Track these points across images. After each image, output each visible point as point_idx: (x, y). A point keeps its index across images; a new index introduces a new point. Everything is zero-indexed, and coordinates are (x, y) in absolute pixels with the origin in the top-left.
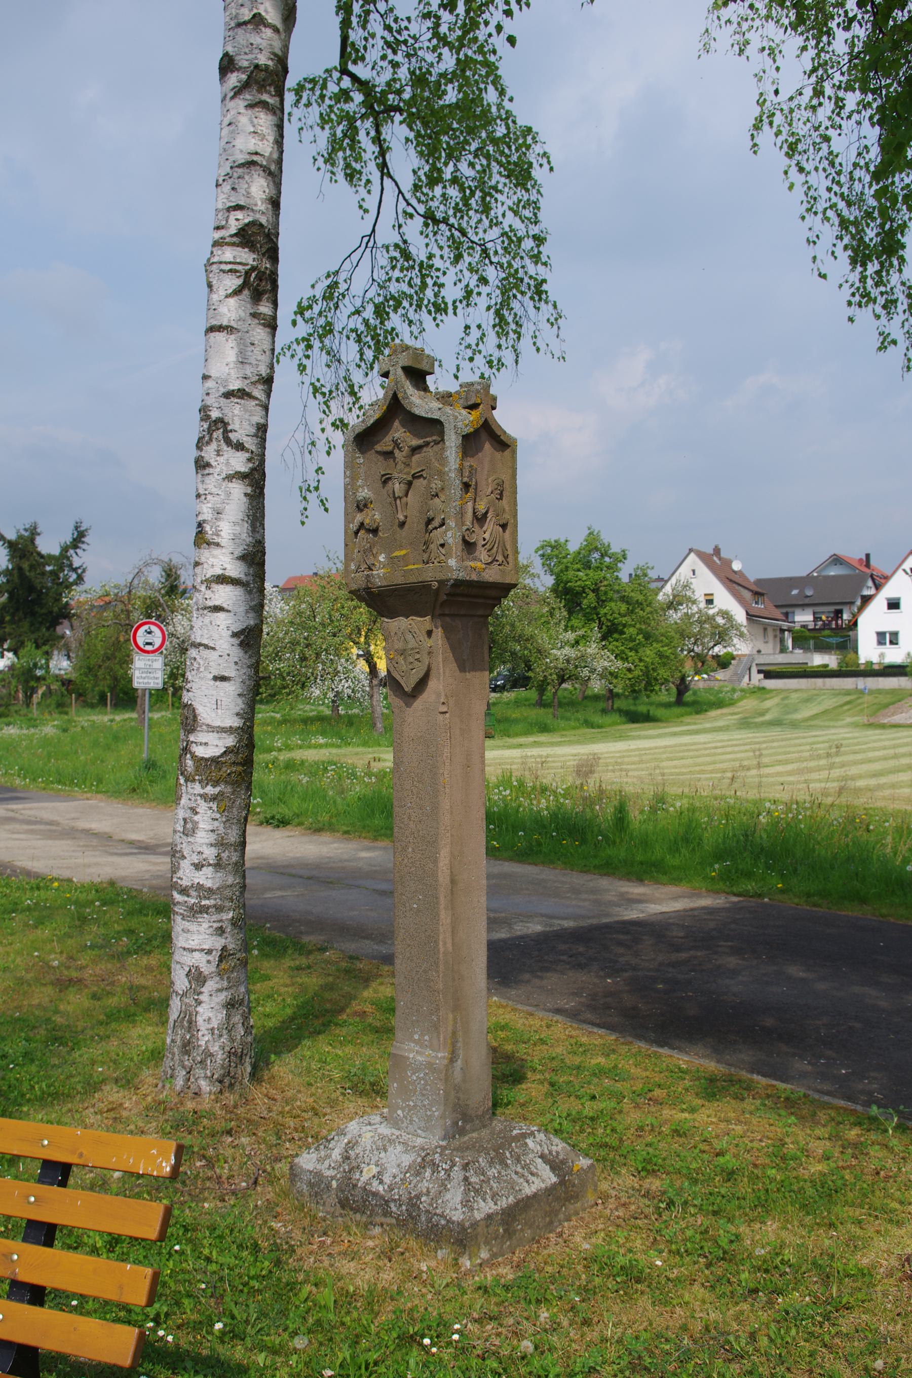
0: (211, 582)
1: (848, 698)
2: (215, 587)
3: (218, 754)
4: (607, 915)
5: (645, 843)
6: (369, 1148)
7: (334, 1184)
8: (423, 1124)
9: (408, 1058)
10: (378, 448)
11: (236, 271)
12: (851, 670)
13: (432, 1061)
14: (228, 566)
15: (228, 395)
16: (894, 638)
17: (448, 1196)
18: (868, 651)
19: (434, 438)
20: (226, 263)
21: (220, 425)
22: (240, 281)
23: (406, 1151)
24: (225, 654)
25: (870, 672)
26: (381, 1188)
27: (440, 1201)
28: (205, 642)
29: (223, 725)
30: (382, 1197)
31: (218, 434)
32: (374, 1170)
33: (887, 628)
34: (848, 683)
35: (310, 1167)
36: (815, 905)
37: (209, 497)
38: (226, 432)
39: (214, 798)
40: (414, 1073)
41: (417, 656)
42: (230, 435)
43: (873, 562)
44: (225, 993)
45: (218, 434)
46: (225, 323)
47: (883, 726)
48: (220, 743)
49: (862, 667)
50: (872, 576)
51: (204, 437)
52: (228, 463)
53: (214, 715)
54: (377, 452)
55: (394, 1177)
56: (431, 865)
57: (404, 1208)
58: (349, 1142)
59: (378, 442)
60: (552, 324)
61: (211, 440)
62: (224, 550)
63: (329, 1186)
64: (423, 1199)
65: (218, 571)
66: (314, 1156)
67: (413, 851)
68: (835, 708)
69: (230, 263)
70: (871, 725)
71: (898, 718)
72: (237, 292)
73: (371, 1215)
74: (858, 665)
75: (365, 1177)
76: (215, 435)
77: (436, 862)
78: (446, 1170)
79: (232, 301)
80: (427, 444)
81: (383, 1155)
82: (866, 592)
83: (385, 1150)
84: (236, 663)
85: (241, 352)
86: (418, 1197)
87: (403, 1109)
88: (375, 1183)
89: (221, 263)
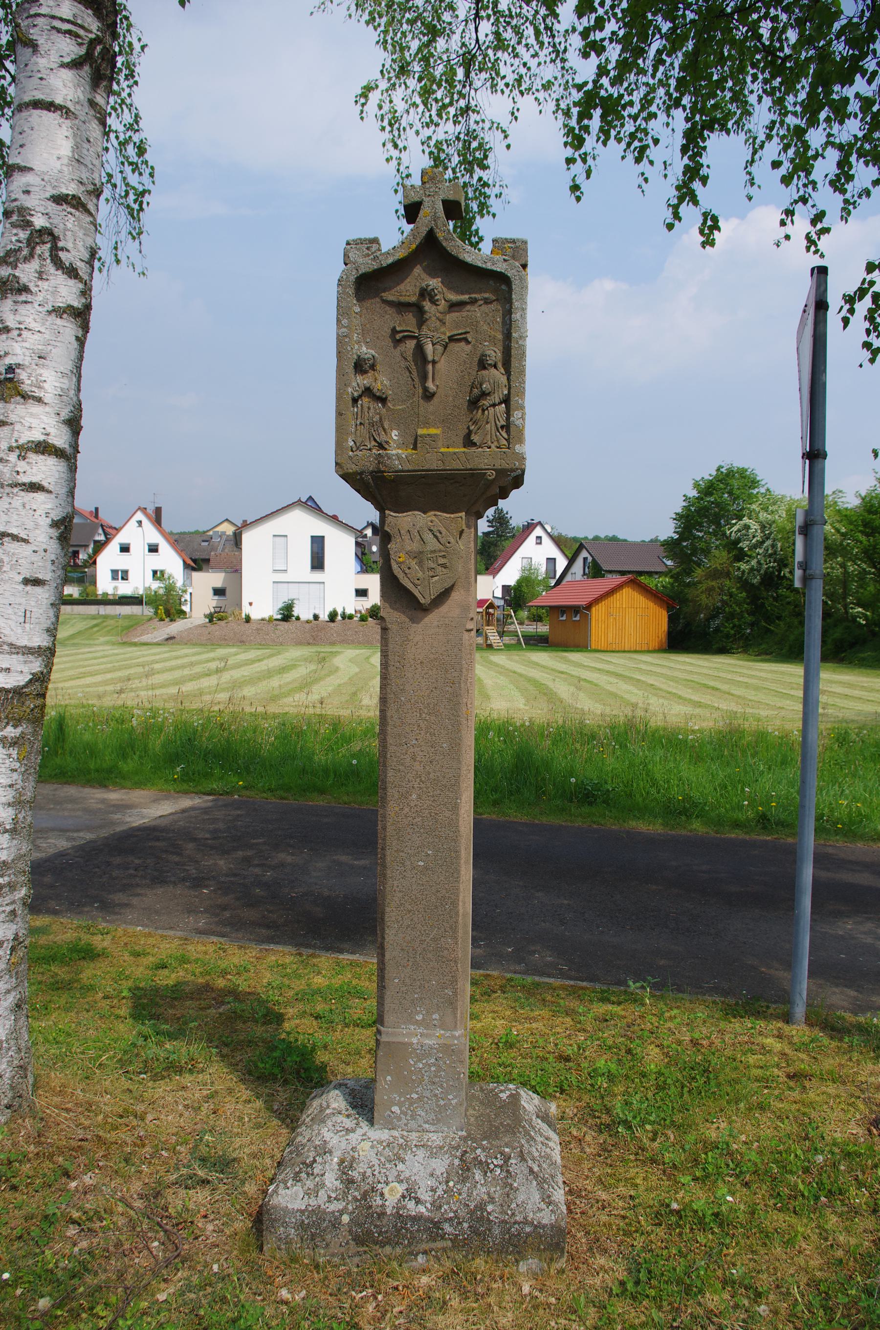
0: (29, 449)
1: (95, 622)
2: (32, 457)
3: (22, 683)
4: (113, 823)
5: (92, 750)
6: (375, 1162)
7: (346, 1219)
8: (433, 1116)
9: (411, 1044)
10: (390, 296)
11: (77, 36)
12: (90, 600)
13: (448, 1042)
14: (53, 431)
15: (59, 199)
16: (125, 575)
17: (521, 1197)
18: (105, 585)
19: (487, 295)
20: (62, 20)
21: (46, 238)
22: (82, 51)
23: (433, 1155)
24: (40, 550)
25: (106, 601)
26: (422, 1209)
27: (513, 1206)
28: (14, 531)
29: (30, 644)
30: (430, 1220)
31: (44, 249)
32: (400, 1189)
33: (120, 567)
34: (92, 610)
35: (299, 1204)
36: (282, 798)
37: (25, 333)
38: (55, 249)
39: (14, 743)
40: (420, 1060)
41: (442, 561)
42: (61, 254)
43: (101, 514)
44: (13, 993)
45: (44, 249)
46: (59, 101)
47: (135, 644)
48: (26, 669)
49: (100, 597)
50: (102, 526)
51: (20, 249)
52: (55, 292)
53: (20, 631)
54: (385, 302)
55: (434, 1190)
56: (448, 814)
57: (465, 1225)
58: (342, 1161)
59: (390, 289)
60: (134, 238)
61: (31, 255)
62: (47, 409)
63: (335, 1224)
64: (490, 1208)
65: (38, 436)
66: (298, 1189)
67: (419, 797)
68: (86, 629)
69: (68, 21)
70: (124, 643)
71: (145, 638)
72: (75, 64)
73: (410, 1244)
74: (97, 595)
75: (391, 1200)
76: (38, 250)
77: (455, 808)
78: (501, 1167)
79: (67, 75)
80: (473, 302)
81: (401, 1166)
82: (97, 538)
83: (403, 1161)
84: (53, 562)
85: (77, 147)
86: (481, 1206)
87: (400, 1105)
88: (411, 1205)
89: (53, 17)
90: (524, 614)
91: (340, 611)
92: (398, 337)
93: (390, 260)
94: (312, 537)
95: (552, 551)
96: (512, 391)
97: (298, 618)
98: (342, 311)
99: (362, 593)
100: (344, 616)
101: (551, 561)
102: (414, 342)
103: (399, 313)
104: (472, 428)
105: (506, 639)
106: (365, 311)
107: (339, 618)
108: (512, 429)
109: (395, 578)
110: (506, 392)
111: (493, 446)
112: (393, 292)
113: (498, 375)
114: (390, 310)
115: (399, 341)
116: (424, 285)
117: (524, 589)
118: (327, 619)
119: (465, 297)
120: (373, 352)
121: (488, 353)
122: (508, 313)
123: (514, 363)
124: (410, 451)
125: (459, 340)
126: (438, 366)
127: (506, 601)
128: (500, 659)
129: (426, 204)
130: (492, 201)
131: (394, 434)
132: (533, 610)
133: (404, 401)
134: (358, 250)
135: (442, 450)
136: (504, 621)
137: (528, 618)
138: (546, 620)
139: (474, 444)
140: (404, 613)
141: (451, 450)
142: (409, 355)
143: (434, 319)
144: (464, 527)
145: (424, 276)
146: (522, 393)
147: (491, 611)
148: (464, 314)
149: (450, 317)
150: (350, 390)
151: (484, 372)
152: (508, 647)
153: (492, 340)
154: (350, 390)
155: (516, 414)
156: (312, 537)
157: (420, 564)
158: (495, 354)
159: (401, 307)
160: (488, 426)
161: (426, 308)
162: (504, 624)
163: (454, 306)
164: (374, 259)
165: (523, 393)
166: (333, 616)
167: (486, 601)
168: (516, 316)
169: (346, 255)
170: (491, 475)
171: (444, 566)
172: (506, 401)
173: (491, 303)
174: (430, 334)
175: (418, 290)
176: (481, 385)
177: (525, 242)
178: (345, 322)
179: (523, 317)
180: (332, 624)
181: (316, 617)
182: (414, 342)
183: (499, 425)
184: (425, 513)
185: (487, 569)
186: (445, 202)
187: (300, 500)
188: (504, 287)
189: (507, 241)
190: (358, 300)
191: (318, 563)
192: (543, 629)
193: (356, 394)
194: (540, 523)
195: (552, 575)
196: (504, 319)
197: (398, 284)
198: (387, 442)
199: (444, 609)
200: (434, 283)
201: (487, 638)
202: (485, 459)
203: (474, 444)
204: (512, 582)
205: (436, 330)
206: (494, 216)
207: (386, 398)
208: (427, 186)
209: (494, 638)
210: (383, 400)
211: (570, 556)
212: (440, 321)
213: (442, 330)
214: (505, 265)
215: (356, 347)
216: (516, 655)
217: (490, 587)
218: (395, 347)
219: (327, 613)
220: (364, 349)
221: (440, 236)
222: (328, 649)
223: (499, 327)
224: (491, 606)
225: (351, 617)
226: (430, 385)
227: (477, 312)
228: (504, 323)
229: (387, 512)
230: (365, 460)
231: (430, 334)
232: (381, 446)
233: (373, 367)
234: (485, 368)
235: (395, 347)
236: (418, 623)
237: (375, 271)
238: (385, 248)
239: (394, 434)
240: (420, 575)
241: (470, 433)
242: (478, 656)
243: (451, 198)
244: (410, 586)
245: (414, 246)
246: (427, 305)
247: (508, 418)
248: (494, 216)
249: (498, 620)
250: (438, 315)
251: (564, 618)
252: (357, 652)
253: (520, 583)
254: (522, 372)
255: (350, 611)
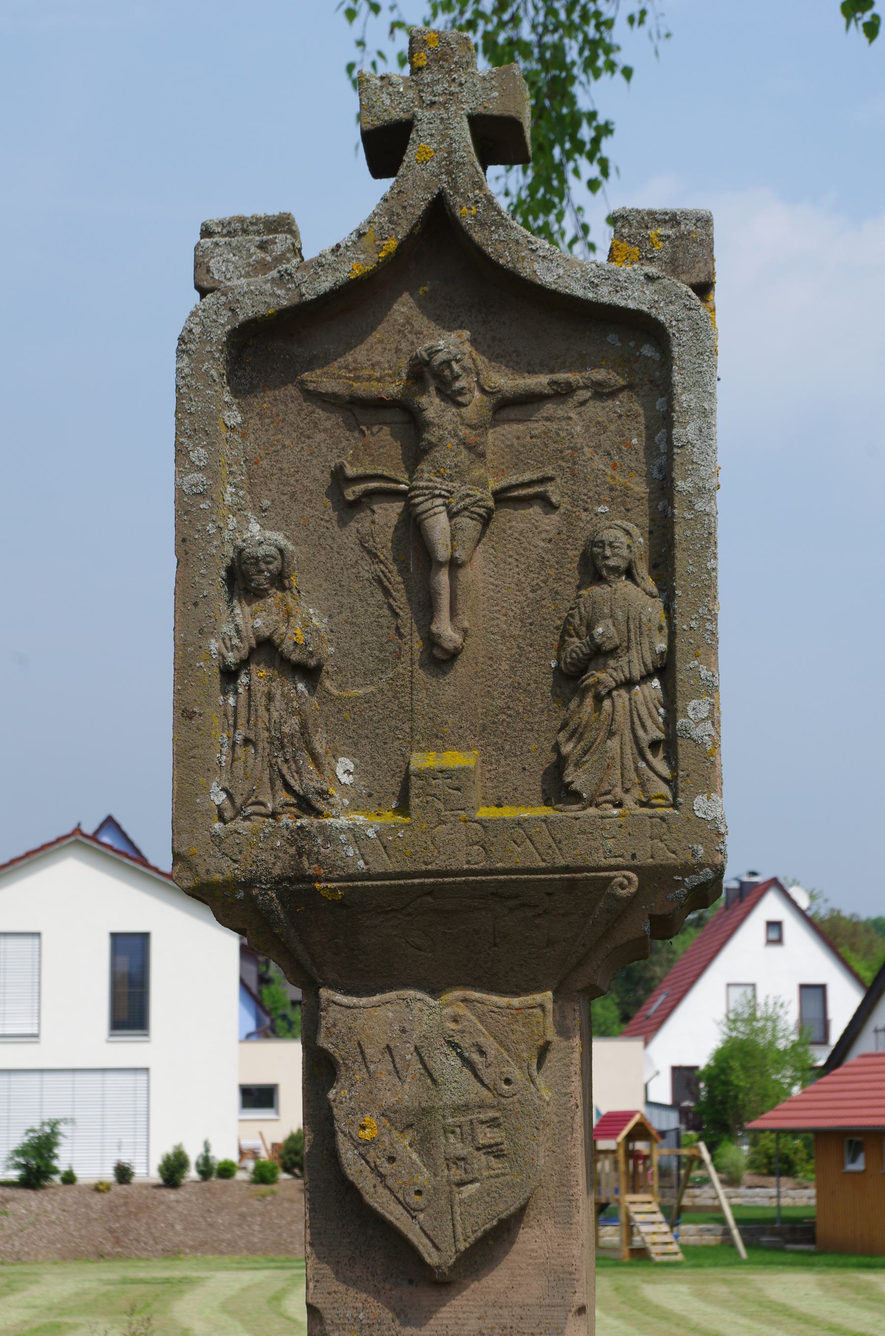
10: (324, 379)
19: (600, 375)
41: (487, 1136)
59: (326, 360)
80: (562, 393)
90: (740, 1152)
91: (194, 1154)
92: (351, 493)
93: (325, 284)
94: (115, 936)
95: (821, 966)
96: (679, 643)
97: (69, 1179)
98: (191, 426)
99: (258, 1097)
100: (206, 1169)
101: (814, 994)
102: (398, 507)
103: (353, 425)
104: (567, 749)
105: (690, 1231)
106: (255, 422)
107: (192, 1174)
108: (683, 749)
109: (349, 1191)
110: (662, 646)
111: (629, 801)
112: (334, 367)
113: (638, 598)
114: (328, 420)
115: (355, 506)
116: (421, 350)
117: (739, 1079)
118: (155, 1177)
119: (539, 381)
120: (278, 537)
121: (608, 535)
122: (662, 421)
123: (684, 563)
124: (389, 818)
125: (525, 501)
126: (466, 575)
127: (684, 1114)
128: (672, 1294)
129: (423, 128)
130: (619, 34)
131: (344, 768)
132: (767, 1142)
133: (369, 675)
134: (236, 250)
135: (485, 813)
136: (678, 1178)
137: (752, 1164)
138: (807, 1172)
139: (575, 797)
140: (377, 1293)
141: (508, 812)
142: (384, 541)
143: (451, 442)
144: (551, 1035)
145: (421, 322)
146: (708, 647)
147: (641, 1146)
148: (538, 427)
149: (498, 438)
150: (214, 645)
151: (597, 590)
152: (696, 1256)
153: (620, 499)
154: (214, 645)
155: (694, 709)
156: (115, 936)
157: (425, 1145)
158: (626, 538)
159: (358, 409)
160: (613, 744)
161: (430, 414)
162: (683, 1184)
163: (508, 406)
164: (284, 278)
165: (713, 649)
166: (173, 1169)
167: (622, 1117)
168: (685, 431)
169: (200, 265)
170: (627, 883)
171: (494, 1151)
172: (664, 669)
173: (613, 394)
174: (441, 486)
175: (404, 362)
176: (590, 627)
177: (705, 221)
178: (199, 454)
179: (706, 434)
180: (171, 1195)
181: (123, 1173)
182: (398, 507)
183: (645, 738)
184: (435, 992)
185: (626, 1018)
186: (477, 122)
187: (78, 831)
188: (647, 351)
189: (654, 218)
190: (235, 393)
191: (130, 1010)
192: (798, 1197)
193: (232, 658)
194: (774, 883)
195: (817, 1034)
196: (650, 438)
197: (350, 347)
198: (323, 794)
199: (495, 1280)
200: (451, 344)
201: (630, 1229)
202: (610, 838)
203: (575, 797)
204: (700, 1057)
205: (459, 474)
206: (628, 73)
207: (319, 668)
208: (427, 77)
209: (652, 1229)
210: (310, 673)
211: (868, 976)
212: (471, 448)
213: (477, 472)
214: (649, 292)
215: (232, 522)
216: (721, 1283)
217: (633, 1075)
218: (343, 523)
219: (156, 1161)
220: (255, 527)
221: (465, 213)
222: (159, 1270)
223: (637, 461)
224: (641, 1131)
225: (226, 1171)
226: (445, 629)
227: (574, 421)
228: (651, 448)
229: (325, 993)
230: (259, 846)
231: (441, 486)
232: (305, 805)
233: (280, 580)
234: (598, 578)
235: (343, 523)
236: (420, 1323)
237: (282, 313)
238: (315, 243)
239: (344, 768)
240: (424, 1177)
241: (560, 764)
242: (605, 1285)
243: (494, 108)
244: (394, 1214)
245: (392, 245)
246: (432, 405)
247: (670, 720)
248: (628, 73)
249: (664, 1173)
250: (463, 432)
251: (859, 1165)
252: (247, 1277)
253: (724, 1059)
254: (707, 588)
255: (224, 1152)
